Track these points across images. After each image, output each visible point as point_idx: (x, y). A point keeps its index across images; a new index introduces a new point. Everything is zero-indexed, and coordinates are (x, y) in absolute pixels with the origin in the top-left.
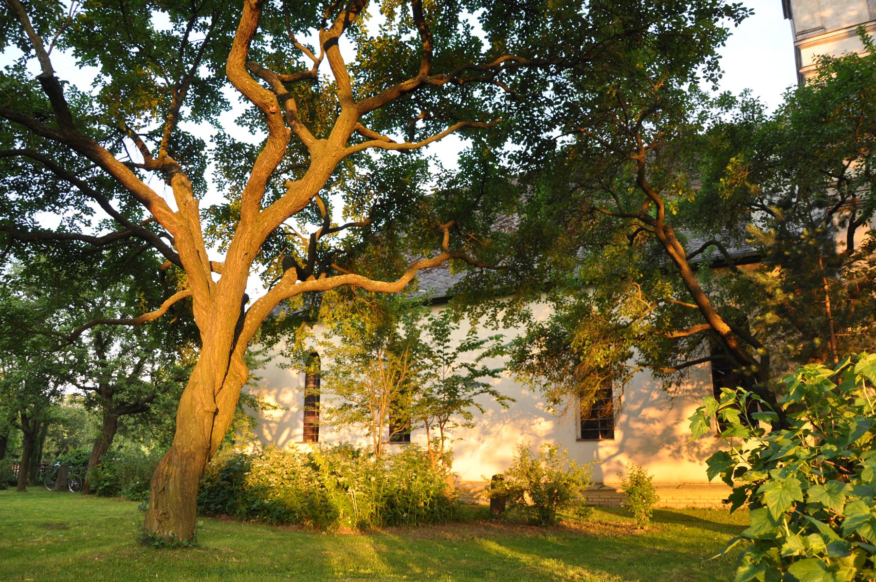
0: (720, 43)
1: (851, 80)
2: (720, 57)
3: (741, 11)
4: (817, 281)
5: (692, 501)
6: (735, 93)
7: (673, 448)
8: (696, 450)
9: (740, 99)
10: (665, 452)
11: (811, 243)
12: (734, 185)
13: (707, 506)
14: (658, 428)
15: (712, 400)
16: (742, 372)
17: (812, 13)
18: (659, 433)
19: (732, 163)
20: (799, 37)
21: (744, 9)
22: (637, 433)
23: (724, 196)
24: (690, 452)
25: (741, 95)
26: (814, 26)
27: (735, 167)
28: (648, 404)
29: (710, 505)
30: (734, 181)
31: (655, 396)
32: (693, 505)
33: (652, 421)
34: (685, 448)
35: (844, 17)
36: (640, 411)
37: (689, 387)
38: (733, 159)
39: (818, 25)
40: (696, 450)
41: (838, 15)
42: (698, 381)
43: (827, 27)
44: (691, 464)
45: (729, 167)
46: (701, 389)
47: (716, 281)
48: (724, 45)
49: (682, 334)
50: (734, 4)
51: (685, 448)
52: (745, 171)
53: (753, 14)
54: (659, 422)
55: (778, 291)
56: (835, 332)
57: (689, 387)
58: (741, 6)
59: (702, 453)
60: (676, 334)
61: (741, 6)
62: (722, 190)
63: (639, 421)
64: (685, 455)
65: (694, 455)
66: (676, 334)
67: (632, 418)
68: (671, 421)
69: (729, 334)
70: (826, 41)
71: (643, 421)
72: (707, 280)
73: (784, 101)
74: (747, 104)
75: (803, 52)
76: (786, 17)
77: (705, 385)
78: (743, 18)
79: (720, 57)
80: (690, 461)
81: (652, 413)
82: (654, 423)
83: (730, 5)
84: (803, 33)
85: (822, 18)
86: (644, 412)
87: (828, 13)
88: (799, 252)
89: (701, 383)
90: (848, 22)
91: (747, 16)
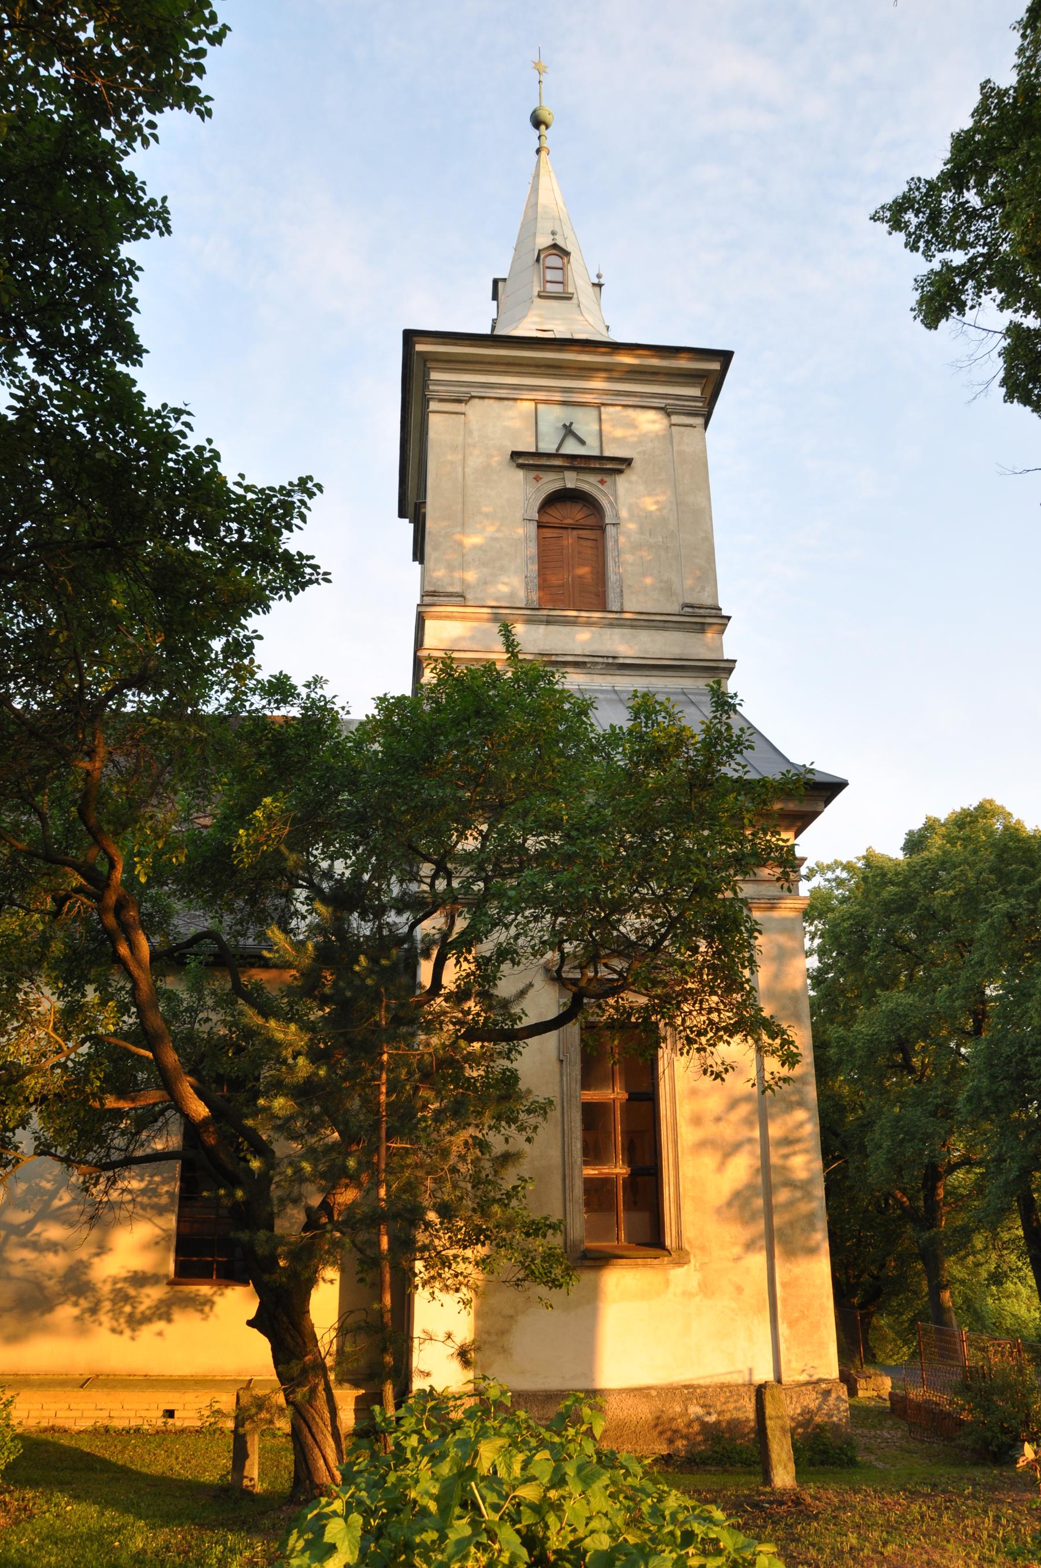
0: (283, 593)
1: (478, 713)
2: (260, 638)
3: (308, 570)
4: (368, 1049)
5: (105, 1414)
6: (298, 680)
7: (84, 1303)
8: (128, 1309)
9: (303, 692)
10: (66, 1313)
11: (369, 982)
12: (262, 844)
13: (133, 1423)
14: (56, 1262)
15: (622, 482)
16: (218, 1198)
17: (451, 568)
18: (61, 1272)
19: (265, 806)
20: (427, 600)
21: (315, 567)
22: (17, 1271)
23: (241, 861)
24: (116, 1313)
25: (307, 686)
26: (450, 589)
27: (269, 817)
28: (47, 1215)
29: (139, 1422)
30: (263, 839)
31: (65, 1197)
32: (106, 1422)
33: (53, 1247)
34: (107, 1305)
35: (491, 590)
36: (30, 1225)
37: (135, 1185)
38: (268, 800)
39: (456, 589)
40: (128, 1309)
41: (485, 583)
42: (152, 1176)
43: (468, 596)
44: (115, 1337)
45: (258, 813)
46: (154, 1191)
47: (214, 993)
48: (289, 598)
49: (125, 1105)
50: (299, 554)
51: (107, 1305)
52: (285, 823)
53: (328, 581)
54: (65, 1249)
55: (301, 1061)
56: (389, 1138)
57: (135, 1185)
58: (311, 562)
59: (138, 1316)
60: (111, 1102)
61: (311, 562)
62: (239, 848)
63: (24, 1245)
64: (105, 1318)
65: (122, 1320)
66: (111, 1102)
67: (14, 1239)
68: (83, 1254)
69: (205, 1121)
70: (464, 618)
71: (35, 1246)
72: (196, 988)
73: (376, 712)
74: (313, 702)
75: (428, 623)
76: (415, 559)
77: (164, 1182)
78: (311, 582)
79: (260, 638)
80: (113, 1330)
81: (54, 1232)
82: (56, 1252)
83: (293, 552)
84: (433, 594)
85: (463, 581)
86: (37, 1229)
87: (471, 576)
88: (348, 994)
89: (157, 1179)
90: (497, 599)
91: (317, 581)
